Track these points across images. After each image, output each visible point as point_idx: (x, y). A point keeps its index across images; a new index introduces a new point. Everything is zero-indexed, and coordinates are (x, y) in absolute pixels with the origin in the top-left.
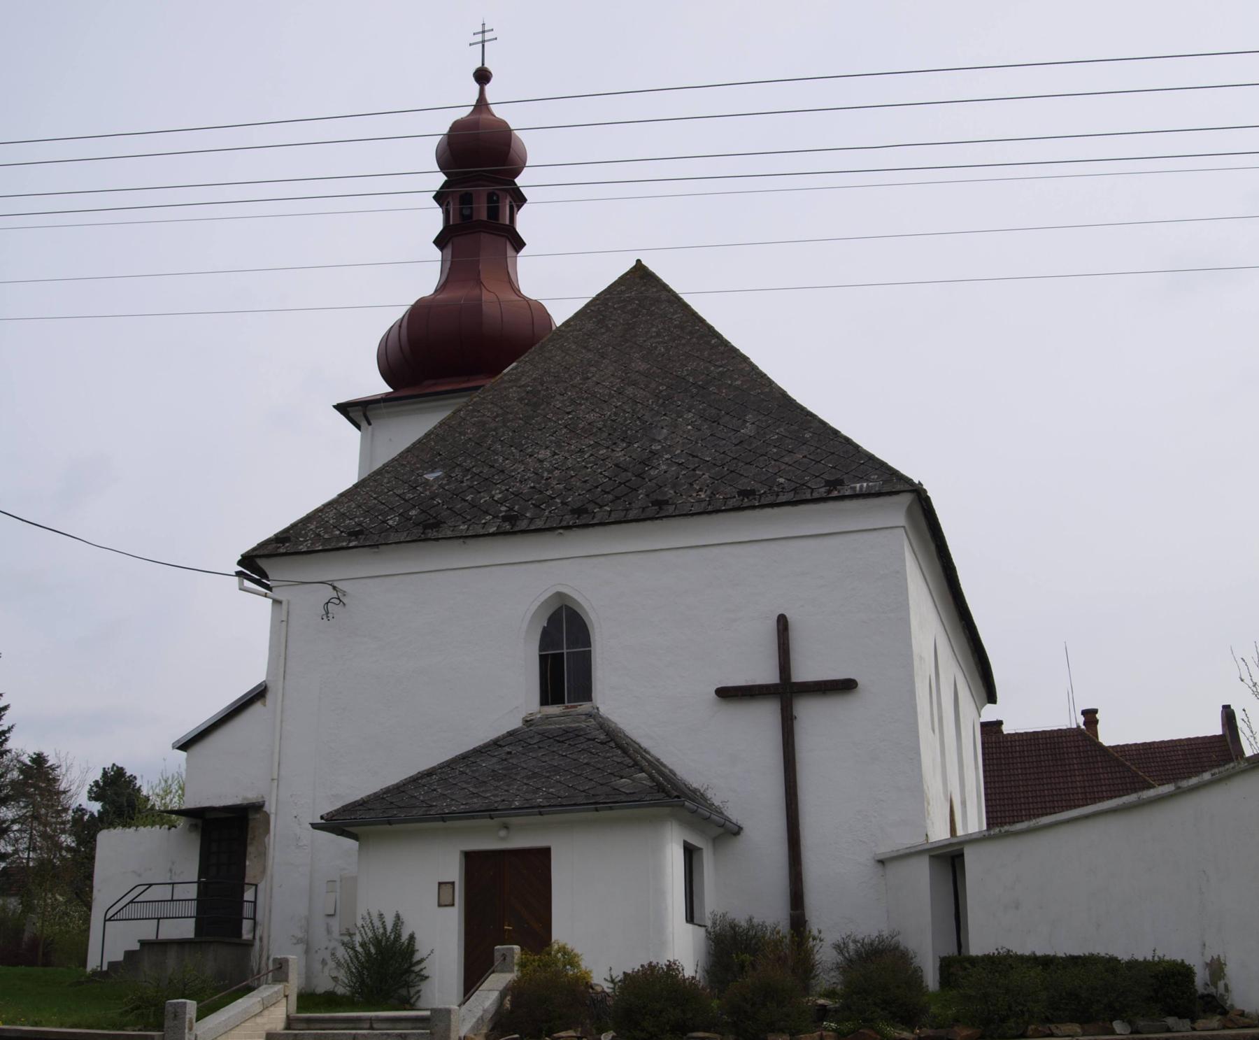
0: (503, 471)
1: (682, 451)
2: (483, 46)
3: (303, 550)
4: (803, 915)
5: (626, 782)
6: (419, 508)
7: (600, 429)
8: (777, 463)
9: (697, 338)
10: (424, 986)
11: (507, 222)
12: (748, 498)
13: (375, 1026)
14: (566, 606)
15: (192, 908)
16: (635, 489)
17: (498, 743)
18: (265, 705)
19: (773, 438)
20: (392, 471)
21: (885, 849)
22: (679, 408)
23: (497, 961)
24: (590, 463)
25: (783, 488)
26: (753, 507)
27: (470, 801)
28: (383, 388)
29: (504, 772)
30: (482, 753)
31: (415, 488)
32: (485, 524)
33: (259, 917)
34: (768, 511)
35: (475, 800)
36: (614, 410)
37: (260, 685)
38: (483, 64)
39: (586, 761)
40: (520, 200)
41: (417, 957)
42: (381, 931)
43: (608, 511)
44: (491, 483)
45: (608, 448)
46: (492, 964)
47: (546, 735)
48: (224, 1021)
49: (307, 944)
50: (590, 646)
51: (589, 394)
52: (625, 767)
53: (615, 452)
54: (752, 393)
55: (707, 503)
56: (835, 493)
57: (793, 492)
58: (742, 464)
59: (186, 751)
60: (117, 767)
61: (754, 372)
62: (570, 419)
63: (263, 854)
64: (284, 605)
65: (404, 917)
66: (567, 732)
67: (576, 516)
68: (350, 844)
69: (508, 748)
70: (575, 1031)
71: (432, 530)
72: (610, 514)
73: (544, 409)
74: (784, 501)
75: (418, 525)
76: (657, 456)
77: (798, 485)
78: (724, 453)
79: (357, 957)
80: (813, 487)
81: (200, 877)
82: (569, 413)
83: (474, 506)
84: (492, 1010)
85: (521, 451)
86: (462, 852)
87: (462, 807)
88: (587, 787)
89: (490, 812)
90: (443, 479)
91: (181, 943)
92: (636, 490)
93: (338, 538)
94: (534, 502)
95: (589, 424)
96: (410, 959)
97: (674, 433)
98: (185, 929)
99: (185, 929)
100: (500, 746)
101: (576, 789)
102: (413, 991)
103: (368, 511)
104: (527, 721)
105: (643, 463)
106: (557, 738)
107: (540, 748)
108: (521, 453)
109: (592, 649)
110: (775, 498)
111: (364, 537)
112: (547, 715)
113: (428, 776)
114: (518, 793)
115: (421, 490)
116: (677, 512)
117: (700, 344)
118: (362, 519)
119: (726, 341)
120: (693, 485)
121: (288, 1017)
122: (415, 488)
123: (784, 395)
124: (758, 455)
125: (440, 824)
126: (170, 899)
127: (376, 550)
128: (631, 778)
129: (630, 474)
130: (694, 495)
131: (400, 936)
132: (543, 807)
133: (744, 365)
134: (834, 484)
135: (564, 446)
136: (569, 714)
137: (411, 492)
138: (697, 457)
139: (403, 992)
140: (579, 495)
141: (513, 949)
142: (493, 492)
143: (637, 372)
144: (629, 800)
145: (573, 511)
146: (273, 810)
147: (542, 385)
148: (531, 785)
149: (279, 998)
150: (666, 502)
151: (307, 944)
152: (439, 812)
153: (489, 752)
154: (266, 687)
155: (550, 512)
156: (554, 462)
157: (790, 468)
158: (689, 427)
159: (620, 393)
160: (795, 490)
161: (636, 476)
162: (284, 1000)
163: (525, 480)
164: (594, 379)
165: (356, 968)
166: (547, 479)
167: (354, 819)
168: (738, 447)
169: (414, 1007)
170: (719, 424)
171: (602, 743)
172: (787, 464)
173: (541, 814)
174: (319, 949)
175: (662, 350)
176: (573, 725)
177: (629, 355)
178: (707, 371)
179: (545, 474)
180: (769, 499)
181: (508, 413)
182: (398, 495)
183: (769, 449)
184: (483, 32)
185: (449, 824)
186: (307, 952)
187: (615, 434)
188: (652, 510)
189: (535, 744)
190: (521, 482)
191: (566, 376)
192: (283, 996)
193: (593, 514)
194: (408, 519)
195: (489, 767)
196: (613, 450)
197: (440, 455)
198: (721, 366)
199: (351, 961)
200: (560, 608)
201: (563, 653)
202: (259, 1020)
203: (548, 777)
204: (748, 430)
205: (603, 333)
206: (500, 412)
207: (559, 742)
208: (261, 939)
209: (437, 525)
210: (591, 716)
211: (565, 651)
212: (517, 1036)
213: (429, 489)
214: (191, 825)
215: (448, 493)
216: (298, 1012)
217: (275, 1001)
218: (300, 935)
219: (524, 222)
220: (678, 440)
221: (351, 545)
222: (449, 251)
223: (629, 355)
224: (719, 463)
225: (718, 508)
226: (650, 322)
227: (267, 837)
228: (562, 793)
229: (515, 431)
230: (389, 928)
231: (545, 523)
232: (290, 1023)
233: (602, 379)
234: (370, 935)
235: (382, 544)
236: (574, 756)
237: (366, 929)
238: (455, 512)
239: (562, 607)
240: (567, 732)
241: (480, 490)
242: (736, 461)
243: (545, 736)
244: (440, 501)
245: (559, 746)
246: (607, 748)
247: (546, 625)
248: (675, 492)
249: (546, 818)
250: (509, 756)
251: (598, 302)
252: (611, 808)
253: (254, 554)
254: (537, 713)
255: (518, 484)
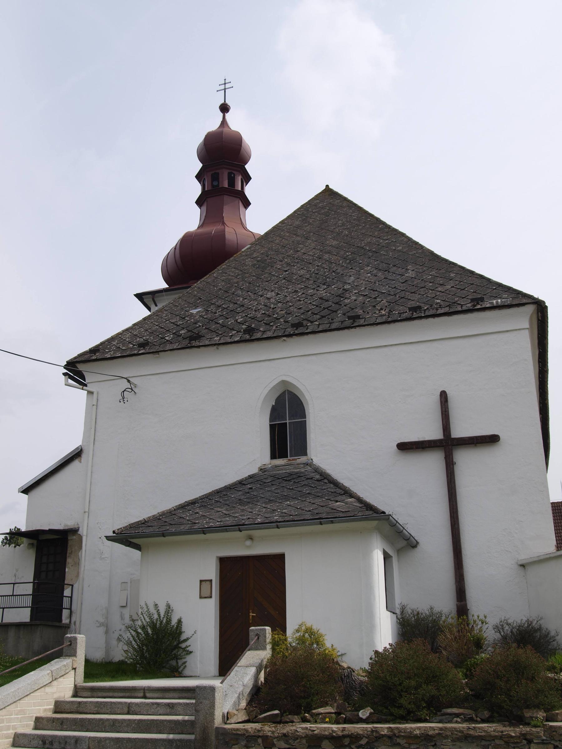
0: (243, 306)
1: (366, 288)
2: (225, 91)
3: (108, 357)
4: (466, 605)
5: (340, 504)
6: (186, 329)
7: (308, 279)
8: (434, 291)
9: (369, 225)
10: (189, 658)
11: (240, 189)
12: (416, 312)
13: (148, 695)
14: (288, 390)
15: (29, 601)
16: (335, 311)
17: (242, 483)
18: (81, 462)
19: (428, 278)
20: (169, 309)
21: (524, 557)
22: (360, 264)
23: (252, 640)
24: (302, 298)
25: (440, 305)
26: (420, 318)
27: (223, 519)
28: (165, 286)
29: (248, 500)
30: (231, 489)
31: (184, 318)
32: (231, 336)
33: (73, 608)
34: (431, 320)
35: (227, 519)
36: (317, 268)
37: (77, 448)
38: (225, 101)
39: (308, 492)
40: (247, 178)
41: (183, 637)
42: (156, 616)
43: (317, 325)
44: (235, 313)
45: (314, 289)
46: (247, 644)
47: (276, 477)
48: (13, 692)
49: (107, 627)
50: (305, 418)
51: (299, 260)
52: (338, 495)
53: (318, 291)
54: (410, 253)
55: (387, 316)
56: (479, 307)
57: (448, 307)
58: (409, 293)
59: (27, 495)
60: (17, 529)
61: (410, 242)
62: (287, 274)
63: (77, 564)
64: (95, 394)
65: (173, 605)
66: (292, 475)
67: (295, 328)
68: (136, 554)
69: (250, 485)
70: (333, 707)
71: (196, 341)
72: (319, 326)
73: (269, 270)
74: (442, 312)
75: (186, 338)
76: (348, 292)
77: (451, 303)
78: (395, 288)
79: (138, 636)
80: (462, 304)
81: (34, 579)
82: (286, 271)
83: (224, 326)
84: (250, 685)
85: (255, 294)
86: (217, 557)
87: (218, 523)
88: (311, 509)
89: (239, 527)
90: (203, 312)
91: (19, 626)
92: (336, 312)
93: (131, 349)
94: (265, 322)
95: (300, 276)
96: (179, 638)
97: (358, 278)
98: (24, 615)
99: (24, 615)
100: (244, 484)
101: (304, 510)
102: (180, 662)
103: (152, 333)
104: (261, 469)
105: (339, 296)
106: (285, 479)
107: (273, 485)
108: (255, 295)
109: (307, 419)
110: (436, 311)
111: (149, 347)
112: (276, 465)
113: (193, 504)
114: (259, 513)
115: (188, 319)
116: (366, 323)
117: (372, 228)
118: (148, 337)
119: (389, 225)
120: (376, 307)
121: (75, 686)
122: (184, 318)
123: (432, 253)
124: (419, 288)
125: (202, 536)
126: (12, 594)
127: (157, 355)
128: (344, 501)
129: (330, 303)
130: (378, 312)
131: (170, 620)
132: (280, 522)
133: (403, 238)
134: (477, 301)
135: (284, 290)
136: (291, 464)
137: (181, 320)
138: (376, 291)
139: (173, 663)
140: (296, 316)
141: (265, 630)
142: (237, 318)
143: (330, 246)
144: (345, 516)
145: (293, 326)
146: (85, 533)
147: (268, 256)
148: (269, 508)
149: (68, 671)
150: (358, 317)
151: (107, 627)
152: (201, 527)
153: (235, 489)
154: (81, 450)
155: (277, 327)
156: (278, 298)
157: (443, 294)
158: (369, 275)
159: (320, 258)
160: (449, 306)
161: (335, 304)
162: (73, 672)
163: (259, 310)
164: (302, 251)
165: (137, 645)
166: (273, 309)
167: (138, 533)
168: (404, 284)
169: (182, 675)
170: (389, 272)
171: (318, 480)
172: (440, 291)
173: (278, 527)
174: (116, 631)
175: (347, 233)
176: (296, 471)
177: (325, 237)
178: (378, 243)
179: (272, 306)
180: (431, 312)
181: (245, 273)
182: (172, 323)
183: (426, 284)
184: (225, 84)
185: (208, 536)
186: (107, 632)
187: (319, 281)
188: (348, 323)
189: (269, 482)
190: (256, 311)
191: (283, 250)
192: (71, 668)
193: (307, 327)
194: (179, 336)
195: (236, 497)
196: (318, 290)
197: (200, 299)
198: (387, 240)
199: (134, 639)
200: (283, 394)
201: (286, 423)
202: (48, 689)
203: (281, 503)
204: (411, 274)
205: (306, 226)
206: (240, 273)
207: (286, 480)
208: (75, 623)
209: (198, 337)
210: (307, 465)
211: (288, 421)
212: (277, 712)
213: (193, 318)
214: (29, 544)
215: (206, 320)
216: (85, 682)
217: (63, 673)
218: (102, 620)
219: (249, 190)
220: (361, 282)
221: (140, 352)
222: (204, 208)
223: (325, 237)
224: (392, 293)
225: (396, 319)
226: (337, 218)
227: (81, 551)
228: (293, 513)
229: (250, 283)
230: (162, 614)
231: (273, 334)
232: (77, 692)
233: (308, 251)
234: (148, 620)
235: (161, 351)
236: (299, 489)
237: (145, 615)
238: (211, 330)
239: (285, 391)
240: (292, 475)
241: (228, 317)
242: (404, 292)
243: (275, 477)
244: (201, 325)
245: (287, 483)
246: (323, 484)
247: (274, 404)
248: (363, 311)
249: (282, 530)
250: (251, 490)
251: (302, 209)
252: (332, 522)
253: (77, 360)
254: (268, 464)
255: (254, 312)
